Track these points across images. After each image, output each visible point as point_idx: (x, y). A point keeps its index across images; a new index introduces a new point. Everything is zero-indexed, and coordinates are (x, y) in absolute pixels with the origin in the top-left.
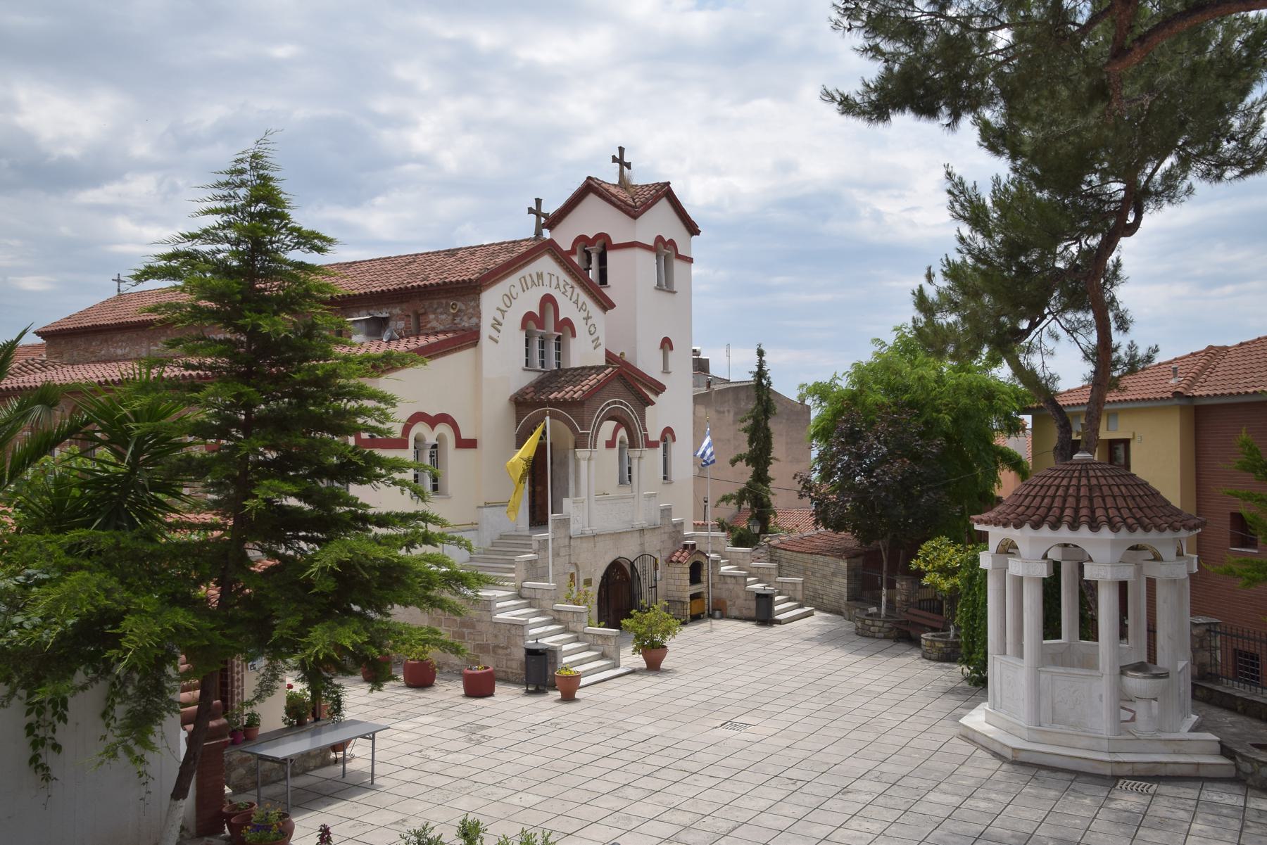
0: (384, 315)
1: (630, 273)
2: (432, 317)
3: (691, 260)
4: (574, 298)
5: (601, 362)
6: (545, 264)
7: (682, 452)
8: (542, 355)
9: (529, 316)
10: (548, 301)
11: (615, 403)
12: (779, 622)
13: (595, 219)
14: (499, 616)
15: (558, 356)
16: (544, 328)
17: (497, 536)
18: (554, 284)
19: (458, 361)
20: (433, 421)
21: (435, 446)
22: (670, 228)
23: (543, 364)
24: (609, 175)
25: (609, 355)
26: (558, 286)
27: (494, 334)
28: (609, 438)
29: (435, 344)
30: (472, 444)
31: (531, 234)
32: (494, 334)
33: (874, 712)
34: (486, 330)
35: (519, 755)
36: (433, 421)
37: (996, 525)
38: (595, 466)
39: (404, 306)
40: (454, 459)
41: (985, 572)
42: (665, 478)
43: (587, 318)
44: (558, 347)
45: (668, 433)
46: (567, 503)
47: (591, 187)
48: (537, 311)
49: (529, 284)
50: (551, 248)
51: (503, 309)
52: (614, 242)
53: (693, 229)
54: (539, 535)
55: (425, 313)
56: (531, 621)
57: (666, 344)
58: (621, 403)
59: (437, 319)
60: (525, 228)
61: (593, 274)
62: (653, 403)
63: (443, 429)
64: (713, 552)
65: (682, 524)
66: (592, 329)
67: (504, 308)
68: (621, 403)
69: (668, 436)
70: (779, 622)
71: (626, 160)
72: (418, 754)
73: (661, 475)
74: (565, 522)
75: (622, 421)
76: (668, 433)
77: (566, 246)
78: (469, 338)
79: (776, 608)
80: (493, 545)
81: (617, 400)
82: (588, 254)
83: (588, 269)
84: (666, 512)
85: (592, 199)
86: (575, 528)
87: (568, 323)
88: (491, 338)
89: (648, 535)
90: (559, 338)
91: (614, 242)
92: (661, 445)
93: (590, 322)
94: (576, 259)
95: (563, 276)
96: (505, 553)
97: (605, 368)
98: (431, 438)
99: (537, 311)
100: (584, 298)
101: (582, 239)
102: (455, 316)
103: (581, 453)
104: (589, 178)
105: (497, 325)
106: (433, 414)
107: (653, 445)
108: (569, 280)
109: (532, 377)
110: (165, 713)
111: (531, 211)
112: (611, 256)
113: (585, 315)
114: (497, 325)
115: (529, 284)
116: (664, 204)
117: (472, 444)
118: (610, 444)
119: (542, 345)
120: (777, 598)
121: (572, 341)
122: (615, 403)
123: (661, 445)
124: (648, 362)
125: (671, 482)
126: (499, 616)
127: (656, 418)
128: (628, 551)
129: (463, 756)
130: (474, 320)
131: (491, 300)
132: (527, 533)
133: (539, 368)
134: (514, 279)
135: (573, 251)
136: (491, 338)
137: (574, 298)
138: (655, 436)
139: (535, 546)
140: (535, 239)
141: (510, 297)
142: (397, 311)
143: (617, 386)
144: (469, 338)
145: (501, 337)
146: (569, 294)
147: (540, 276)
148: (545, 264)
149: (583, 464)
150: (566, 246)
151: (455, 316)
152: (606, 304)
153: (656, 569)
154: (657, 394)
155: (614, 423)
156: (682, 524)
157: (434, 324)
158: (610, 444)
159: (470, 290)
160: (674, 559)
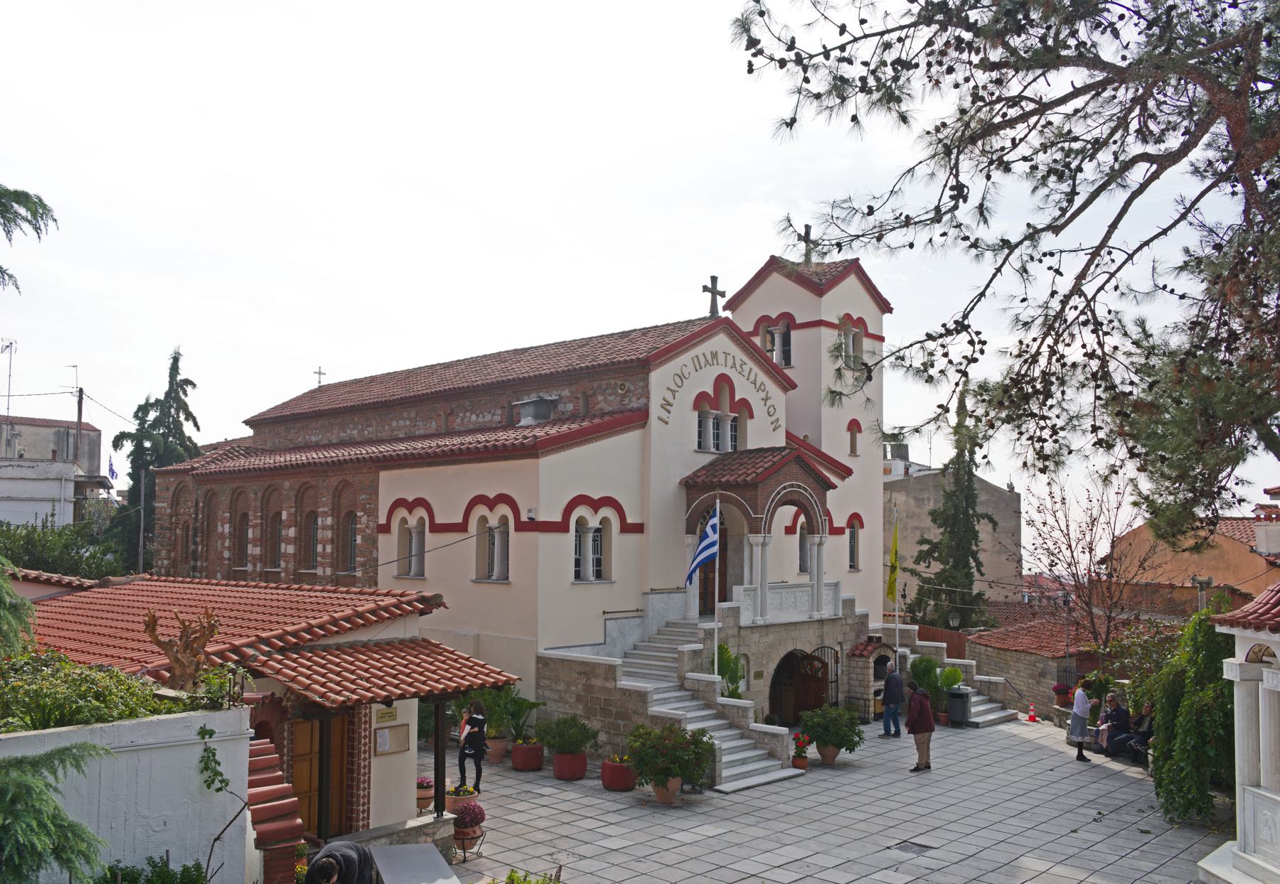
0: (554, 397)
1: (815, 354)
2: (600, 398)
3: (882, 339)
4: (752, 377)
5: (781, 442)
6: (721, 342)
7: (872, 538)
8: (717, 437)
9: (701, 399)
10: (723, 382)
11: (792, 486)
12: (976, 725)
13: (784, 297)
14: (655, 709)
15: (734, 439)
16: (720, 406)
17: (663, 623)
18: (730, 363)
19: (627, 441)
20: (596, 505)
21: (598, 530)
22: (862, 307)
23: (717, 447)
24: (795, 255)
25: (789, 435)
26: (734, 366)
27: (664, 415)
28: (789, 523)
29: (599, 425)
30: (639, 528)
31: (706, 313)
32: (664, 415)
33: (1086, 841)
34: (655, 411)
35: (657, 866)
36: (596, 505)
37: (1245, 627)
38: (775, 550)
39: (574, 388)
40: (618, 542)
41: (1231, 683)
42: (851, 567)
43: (766, 399)
44: (734, 429)
45: (855, 521)
46: (737, 591)
47: (774, 264)
48: (711, 392)
49: (703, 363)
50: (729, 327)
51: (673, 388)
52: (798, 321)
53: (885, 307)
54: (708, 625)
55: (594, 394)
56: (690, 715)
57: (854, 426)
58: (800, 487)
59: (605, 400)
60: (699, 308)
61: (776, 357)
62: (835, 487)
63: (606, 512)
64: (901, 645)
65: (866, 616)
66: (772, 410)
67: (676, 388)
68: (800, 487)
69: (856, 523)
70: (976, 725)
71: (720, 288)
72: (548, 858)
73: (848, 563)
74: (736, 612)
75: (803, 508)
76: (855, 521)
77: (747, 327)
78: (639, 418)
79: (973, 710)
80: (659, 633)
81: (793, 482)
82: (772, 335)
83: (772, 351)
84: (850, 603)
85: (776, 278)
86: (745, 620)
87: (744, 403)
88: (660, 419)
89: (826, 629)
90: (735, 420)
91: (798, 321)
92: (847, 531)
93: (769, 403)
94: (757, 340)
95: (740, 355)
96: (670, 642)
97: (784, 448)
98: (594, 522)
99: (711, 392)
100: (762, 377)
101: (764, 319)
102: (623, 396)
103: (757, 539)
104: (773, 257)
105: (666, 405)
106: (596, 497)
107: (838, 531)
108: (746, 359)
109: (706, 459)
110: (942, 530)
111: (705, 289)
112: (794, 334)
113: (763, 395)
114: (666, 405)
115: (703, 363)
116: (852, 280)
117: (639, 528)
118: (790, 530)
119: (717, 426)
120: (974, 699)
121: (749, 422)
122: (792, 486)
123: (847, 531)
124: (834, 445)
125: (858, 571)
126: (655, 709)
127: (839, 503)
128: (806, 643)
129: (595, 862)
130: (643, 400)
131: (659, 378)
132: (696, 621)
133: (713, 450)
134: (685, 358)
135: (755, 333)
136: (660, 419)
137: (752, 377)
138: (840, 521)
139: (702, 635)
140: (711, 318)
141: (682, 377)
142: (566, 393)
143: (794, 468)
144: (639, 418)
145: (672, 418)
146: (746, 373)
147: (714, 355)
148: (721, 342)
149: (757, 551)
150: (747, 327)
151: (623, 396)
152: (788, 385)
153: (837, 662)
154: (843, 478)
155: (794, 509)
156: (866, 616)
157: (603, 405)
158: (790, 530)
159: (644, 366)
160: (857, 653)
